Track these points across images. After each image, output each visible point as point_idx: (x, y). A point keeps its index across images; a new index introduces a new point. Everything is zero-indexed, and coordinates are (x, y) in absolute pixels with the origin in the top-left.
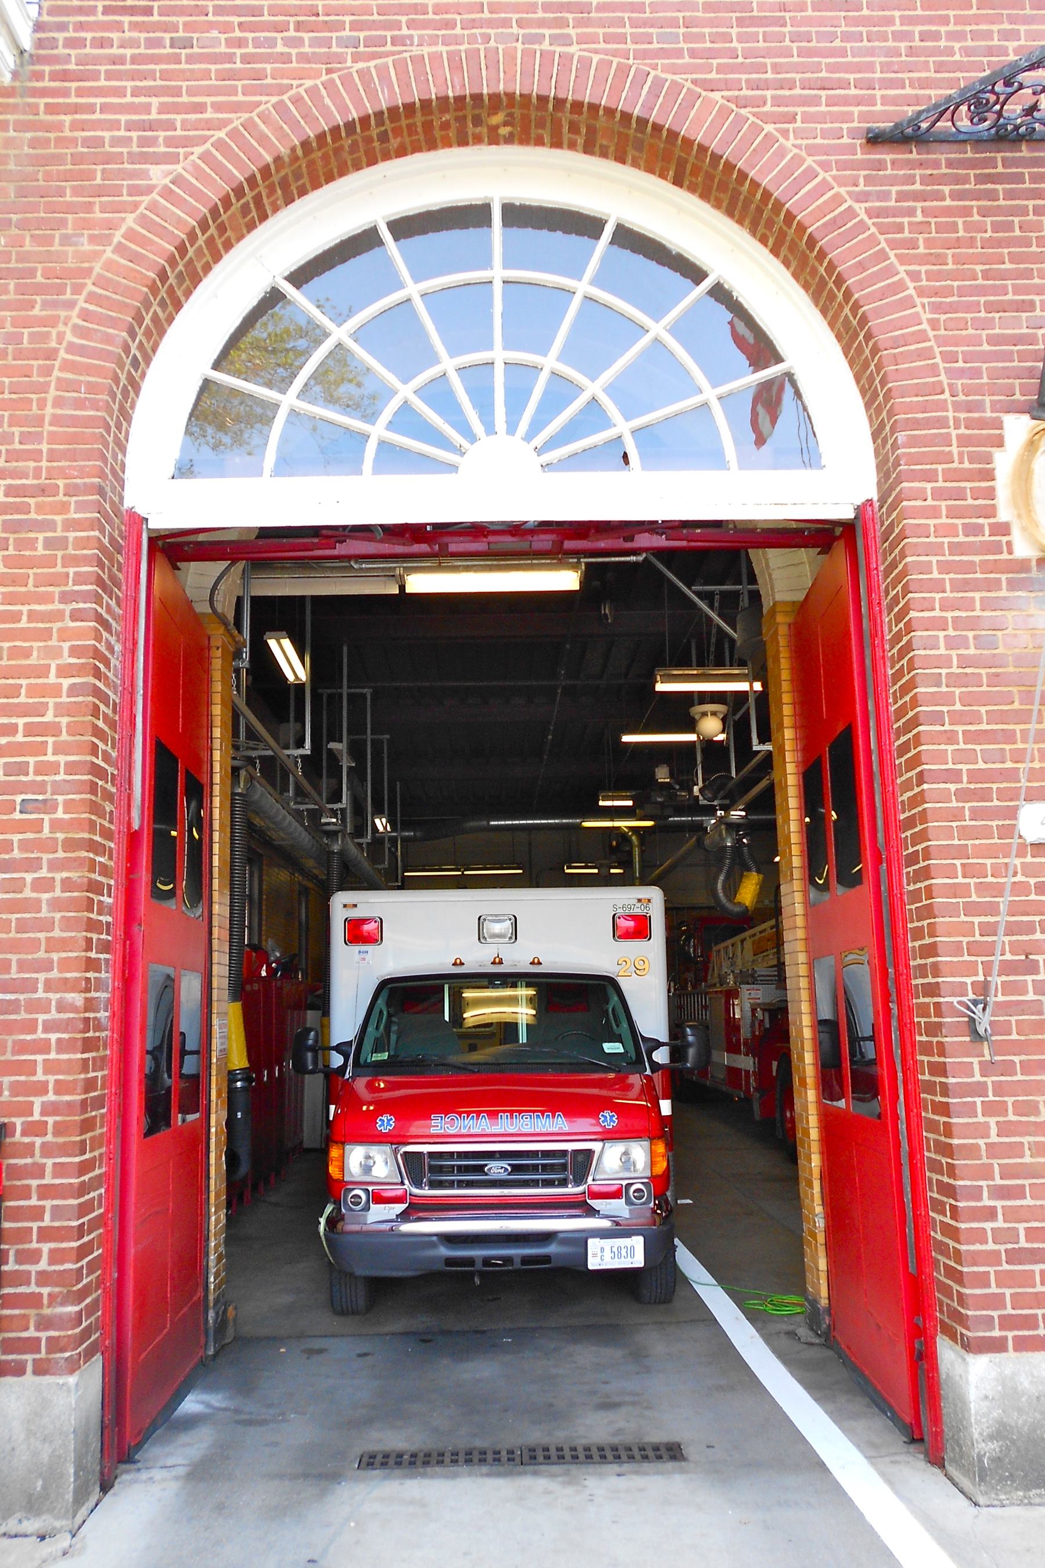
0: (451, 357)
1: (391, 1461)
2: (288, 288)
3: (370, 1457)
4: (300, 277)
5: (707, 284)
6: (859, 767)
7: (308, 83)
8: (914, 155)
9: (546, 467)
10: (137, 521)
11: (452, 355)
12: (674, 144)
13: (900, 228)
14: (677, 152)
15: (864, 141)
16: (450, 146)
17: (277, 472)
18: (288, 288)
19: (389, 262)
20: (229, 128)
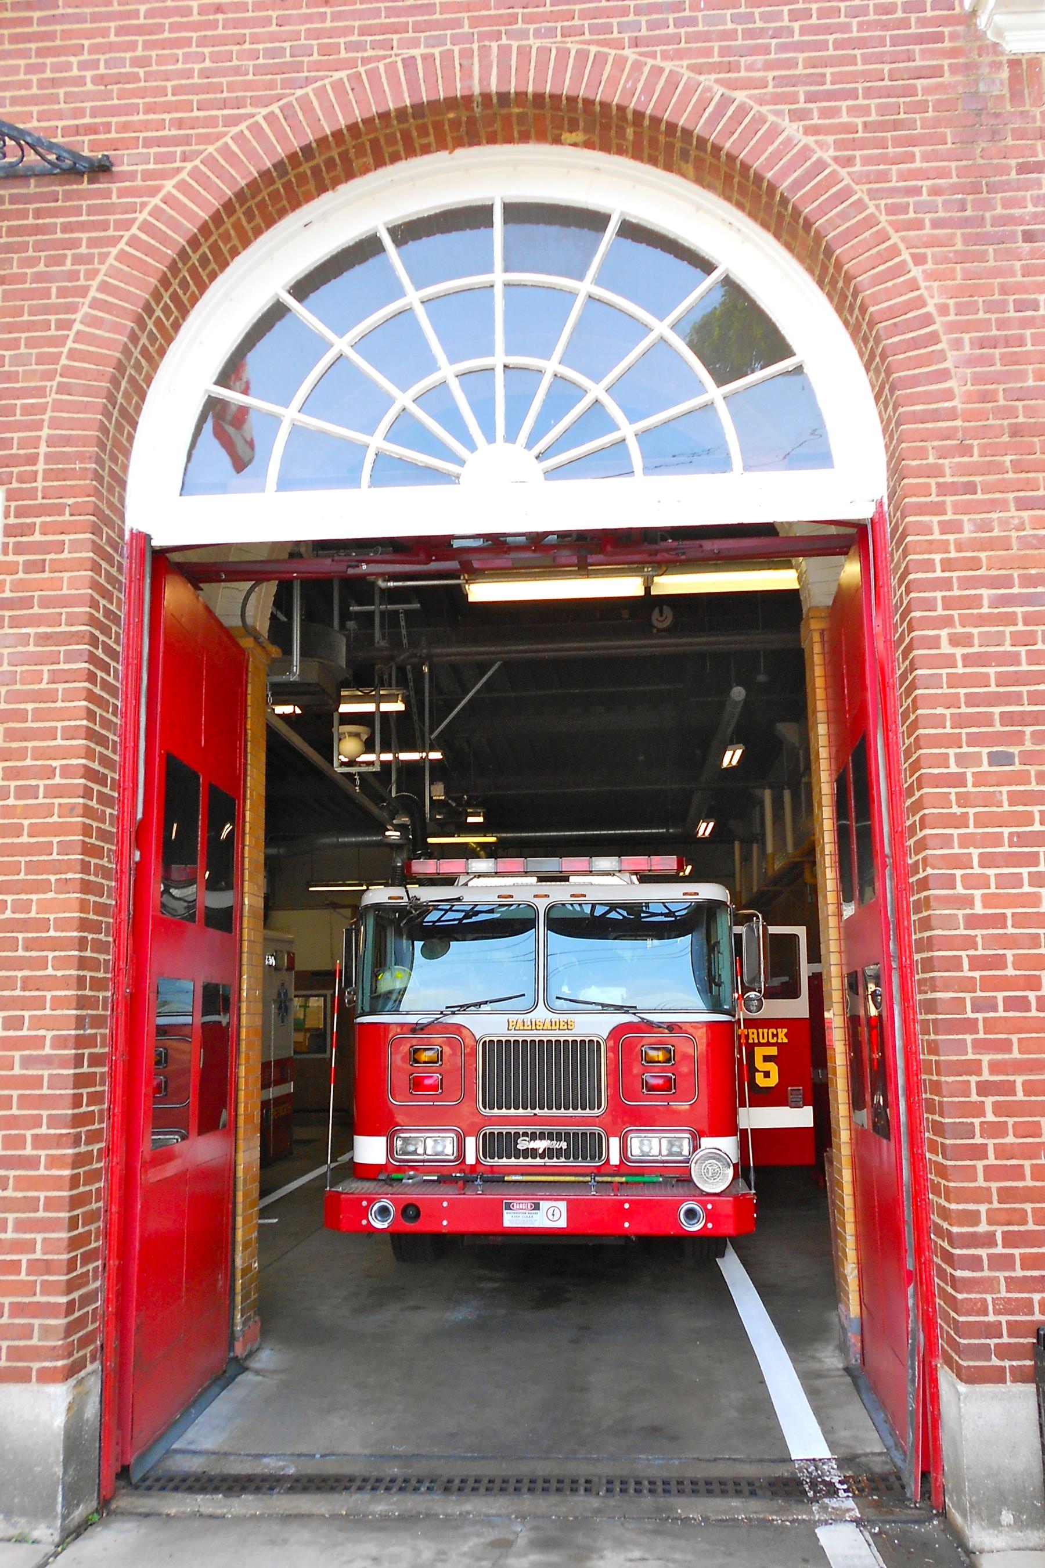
0: (549, 359)
1: (498, 1484)
2: (290, 301)
3: (545, 1482)
4: (302, 289)
5: (716, 276)
6: (159, 784)
7: (299, 92)
8: (85, 185)
9: (551, 474)
10: (142, 539)
11: (548, 358)
12: (658, 130)
13: (905, 209)
14: (662, 139)
15: (114, 169)
16: (479, 144)
17: (284, 484)
18: (290, 301)
19: (390, 268)
20: (219, 144)
